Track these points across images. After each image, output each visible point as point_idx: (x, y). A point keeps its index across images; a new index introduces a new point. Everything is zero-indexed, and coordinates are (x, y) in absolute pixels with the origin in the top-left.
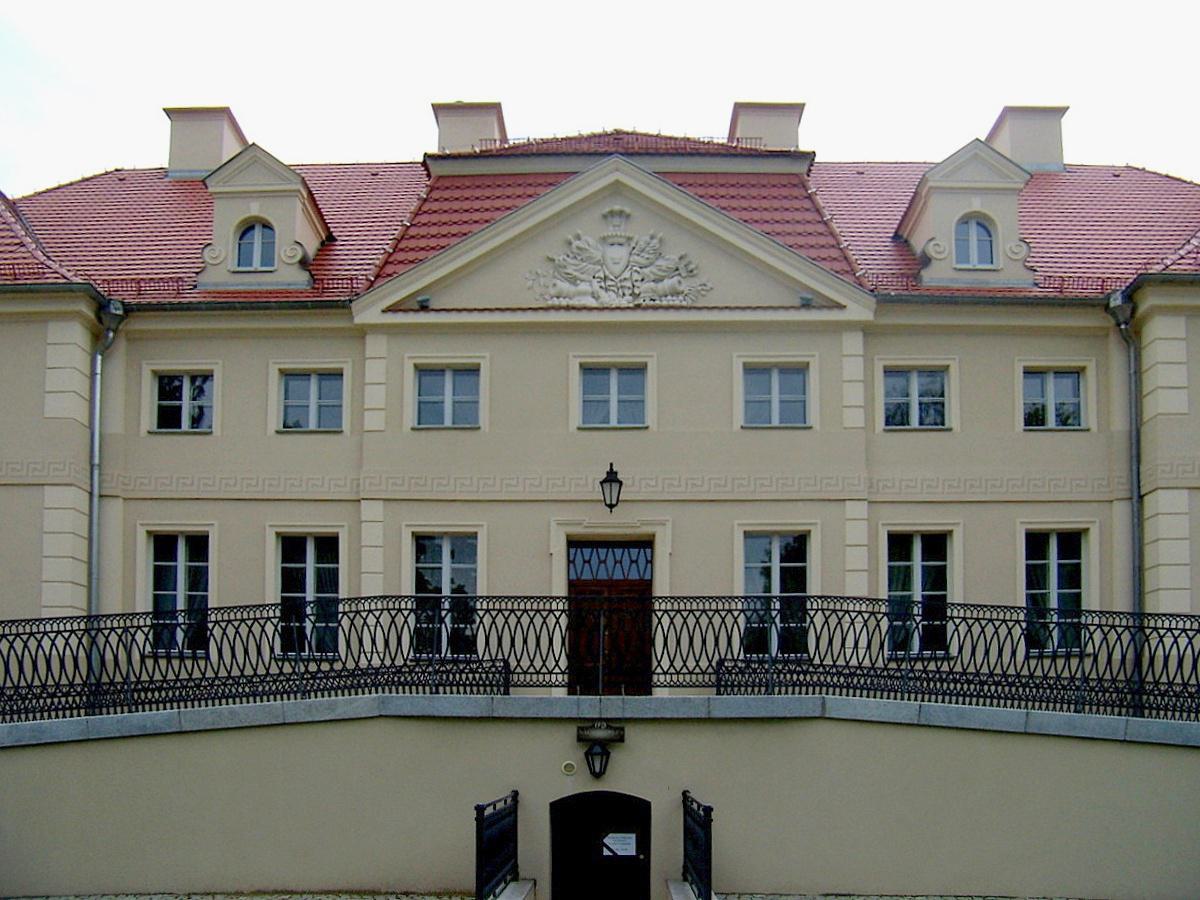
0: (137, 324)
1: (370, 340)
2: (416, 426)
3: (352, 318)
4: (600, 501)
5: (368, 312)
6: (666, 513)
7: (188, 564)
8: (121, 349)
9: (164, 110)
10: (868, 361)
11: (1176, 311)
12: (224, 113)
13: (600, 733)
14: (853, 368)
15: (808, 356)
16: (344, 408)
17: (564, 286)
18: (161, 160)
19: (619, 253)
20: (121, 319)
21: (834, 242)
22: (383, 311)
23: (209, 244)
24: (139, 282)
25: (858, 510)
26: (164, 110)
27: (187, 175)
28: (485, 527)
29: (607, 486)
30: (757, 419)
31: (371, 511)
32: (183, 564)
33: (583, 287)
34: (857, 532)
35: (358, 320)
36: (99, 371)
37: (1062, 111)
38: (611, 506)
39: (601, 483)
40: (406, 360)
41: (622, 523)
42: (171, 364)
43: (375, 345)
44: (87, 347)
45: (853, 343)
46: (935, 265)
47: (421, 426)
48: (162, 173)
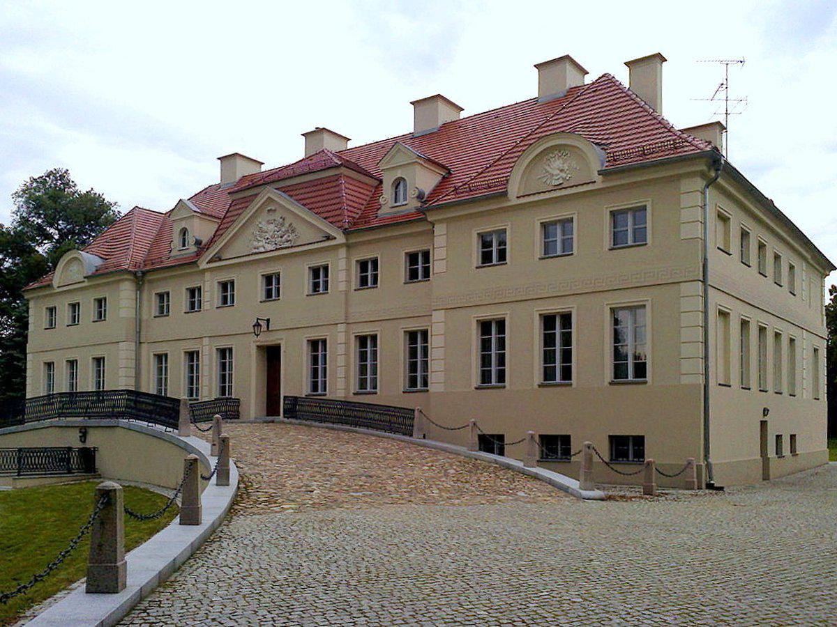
0: (149, 277)
1: (206, 274)
2: (543, 256)
3: (198, 267)
4: (252, 333)
5: (203, 265)
6: (283, 335)
7: (498, 336)
8: (146, 287)
9: (535, 66)
10: (348, 258)
11: (440, 221)
12: (567, 58)
13: (83, 430)
14: (342, 264)
15: (572, 214)
16: (648, 229)
17: (256, 243)
18: (534, 93)
19: (271, 227)
20: (143, 277)
21: (662, 126)
22: (207, 263)
23: (172, 241)
24: (643, 147)
25: (342, 328)
26: (535, 66)
27: (550, 99)
28: (650, 301)
29: (256, 328)
30: (618, 241)
31: (438, 316)
32: (559, 331)
33: (261, 244)
34: (341, 338)
35: (201, 268)
36: (138, 297)
37: (463, 110)
38: (257, 335)
39: (254, 326)
40: (536, 221)
41: (268, 339)
42: (160, 291)
43: (208, 275)
44: (134, 289)
45: (342, 252)
46: (383, 207)
47: (547, 256)
48: (534, 101)
